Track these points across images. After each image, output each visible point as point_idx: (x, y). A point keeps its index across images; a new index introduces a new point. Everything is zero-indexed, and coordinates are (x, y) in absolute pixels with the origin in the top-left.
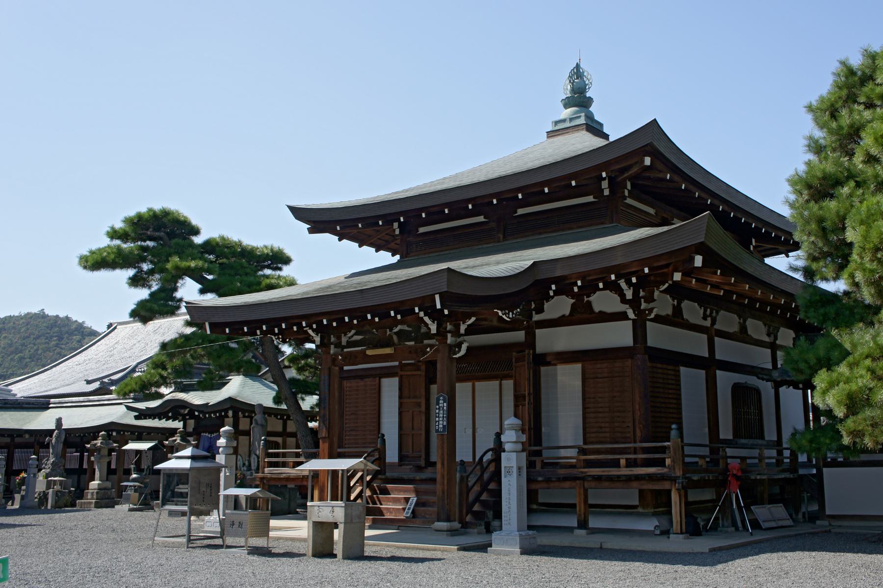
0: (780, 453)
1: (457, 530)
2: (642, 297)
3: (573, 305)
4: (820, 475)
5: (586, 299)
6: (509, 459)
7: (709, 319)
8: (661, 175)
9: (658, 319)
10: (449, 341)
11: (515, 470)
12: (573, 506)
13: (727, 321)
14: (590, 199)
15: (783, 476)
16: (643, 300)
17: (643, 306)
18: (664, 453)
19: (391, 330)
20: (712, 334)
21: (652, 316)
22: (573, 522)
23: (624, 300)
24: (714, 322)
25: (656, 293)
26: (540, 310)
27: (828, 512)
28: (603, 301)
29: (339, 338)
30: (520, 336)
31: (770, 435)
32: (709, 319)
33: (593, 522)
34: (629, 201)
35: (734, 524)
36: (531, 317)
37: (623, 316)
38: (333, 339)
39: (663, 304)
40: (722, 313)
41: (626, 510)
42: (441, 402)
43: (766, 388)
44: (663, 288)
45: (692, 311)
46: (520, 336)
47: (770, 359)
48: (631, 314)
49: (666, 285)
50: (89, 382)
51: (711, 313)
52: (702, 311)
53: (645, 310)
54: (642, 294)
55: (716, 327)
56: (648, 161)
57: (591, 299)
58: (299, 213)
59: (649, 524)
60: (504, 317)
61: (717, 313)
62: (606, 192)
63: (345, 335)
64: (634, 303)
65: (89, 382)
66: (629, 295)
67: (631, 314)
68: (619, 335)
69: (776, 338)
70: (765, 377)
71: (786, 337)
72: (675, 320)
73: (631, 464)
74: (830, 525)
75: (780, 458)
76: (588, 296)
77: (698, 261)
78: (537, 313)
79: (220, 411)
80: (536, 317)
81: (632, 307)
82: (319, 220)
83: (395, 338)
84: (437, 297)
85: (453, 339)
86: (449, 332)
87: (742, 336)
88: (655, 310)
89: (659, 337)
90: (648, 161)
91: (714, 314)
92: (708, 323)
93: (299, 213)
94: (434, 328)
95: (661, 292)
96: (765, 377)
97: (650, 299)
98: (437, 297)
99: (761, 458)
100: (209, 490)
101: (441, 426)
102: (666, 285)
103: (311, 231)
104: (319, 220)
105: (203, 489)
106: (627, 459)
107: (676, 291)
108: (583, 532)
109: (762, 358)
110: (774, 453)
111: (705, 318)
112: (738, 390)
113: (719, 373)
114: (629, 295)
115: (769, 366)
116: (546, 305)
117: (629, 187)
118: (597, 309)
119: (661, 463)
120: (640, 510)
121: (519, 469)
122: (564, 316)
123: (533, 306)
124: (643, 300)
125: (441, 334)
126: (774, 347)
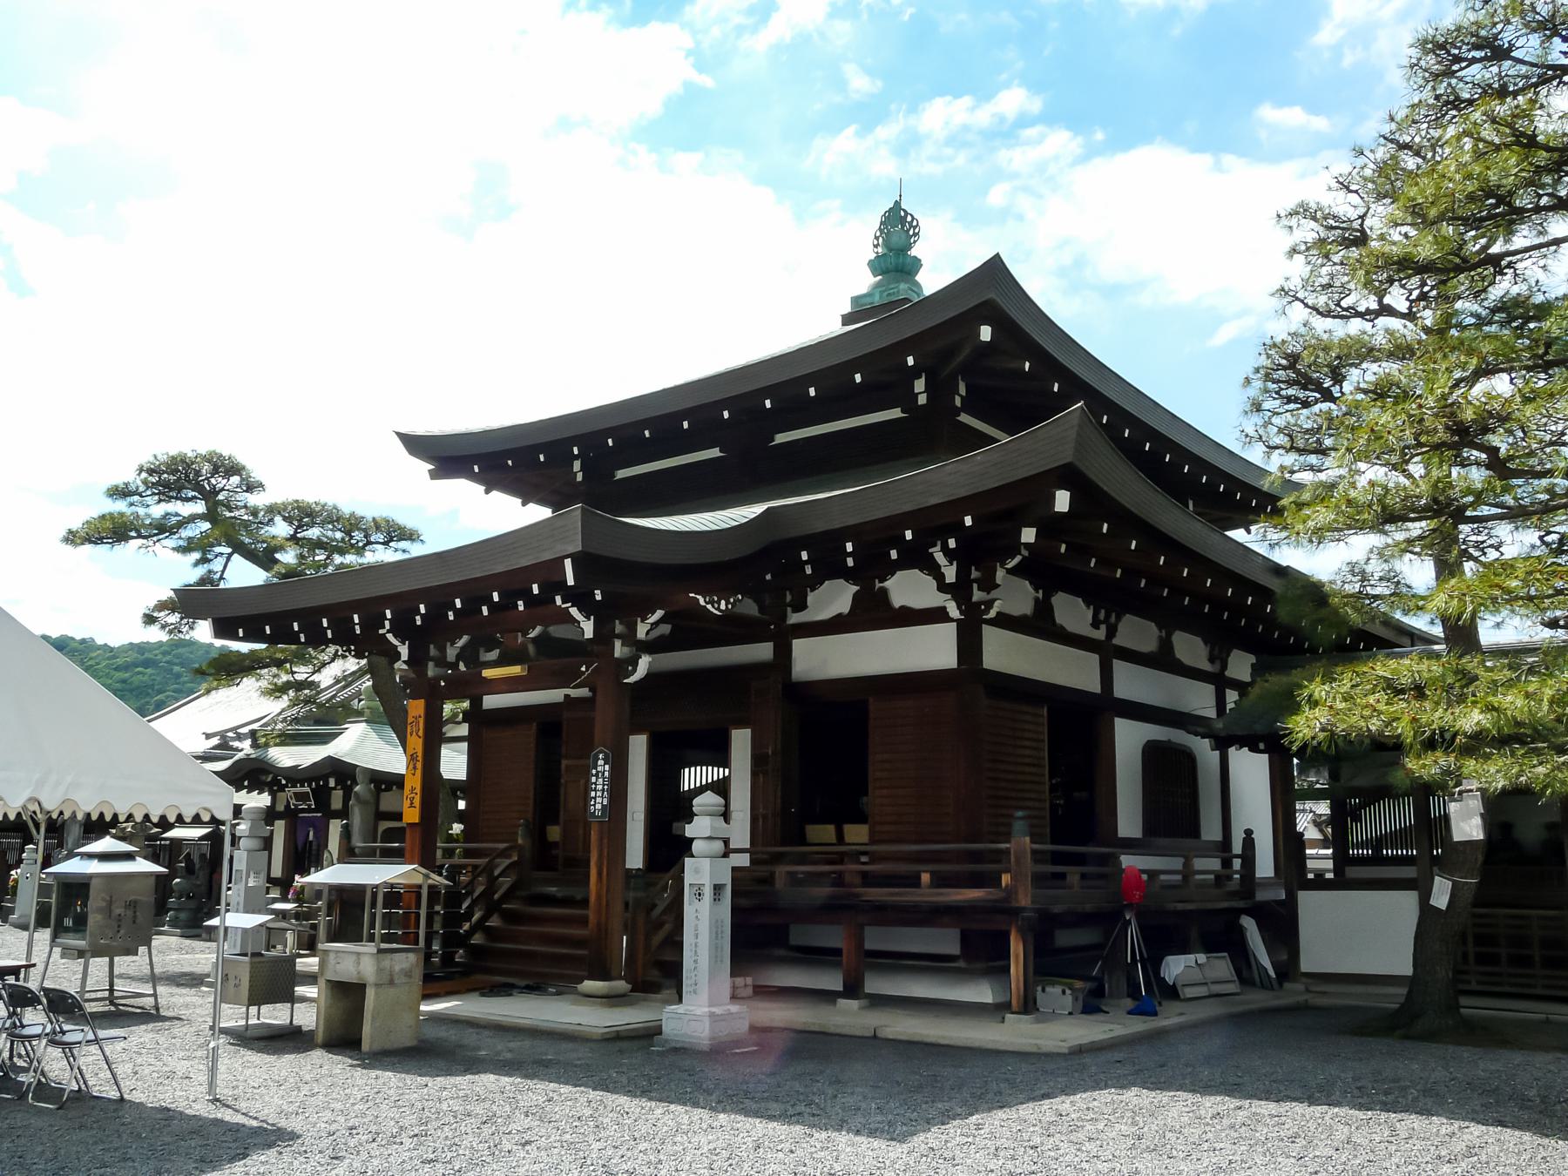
0: (1227, 863)
1: (624, 995)
2: (975, 581)
3: (856, 596)
4: (1291, 905)
5: (878, 585)
6: (697, 871)
7: (1103, 627)
8: (1013, 365)
9: (1003, 621)
10: (617, 654)
11: (708, 892)
12: (837, 952)
13: (1137, 633)
14: (895, 413)
15: (1225, 905)
16: (975, 586)
17: (977, 595)
18: (999, 862)
19: (525, 634)
20: (1108, 653)
21: (992, 614)
22: (832, 981)
23: (943, 587)
24: (1112, 632)
25: (1000, 574)
26: (801, 606)
27: (1306, 965)
28: (909, 588)
29: (443, 650)
30: (763, 651)
31: (1211, 830)
32: (1103, 627)
33: (876, 984)
34: (964, 418)
35: (1134, 992)
36: (784, 617)
37: (938, 615)
38: (433, 651)
39: (1015, 596)
40: (1128, 617)
41: (933, 964)
42: (601, 762)
43: (1203, 748)
44: (1011, 564)
45: (1072, 612)
46: (763, 651)
47: (1213, 702)
48: (954, 611)
49: (1018, 559)
50: (208, 736)
51: (1108, 616)
52: (1090, 613)
53: (979, 604)
54: (975, 574)
55: (1115, 641)
56: (986, 333)
57: (887, 584)
58: (416, 444)
59: (981, 993)
60: (709, 607)
61: (1119, 618)
62: (922, 400)
63: (453, 644)
64: (958, 591)
65: (208, 736)
66: (950, 574)
67: (954, 611)
68: (933, 649)
69: (1224, 667)
70: (1200, 730)
71: (1240, 666)
72: (1040, 624)
73: (940, 881)
74: (1308, 991)
75: (1228, 872)
76: (883, 580)
77: (1062, 501)
78: (795, 611)
79: (317, 779)
80: (794, 618)
81: (954, 598)
82: (450, 456)
83: (531, 649)
84: (568, 563)
85: (626, 649)
86: (618, 637)
87: (1162, 660)
88: (997, 603)
89: (1005, 653)
90: (986, 333)
91: (1113, 619)
92: (1100, 634)
93: (416, 444)
94: (588, 628)
95: (1009, 571)
96: (1200, 730)
97: (989, 584)
98: (568, 563)
99: (1187, 872)
100: (130, 913)
101: (599, 806)
102: (1018, 559)
103: (434, 475)
104: (450, 456)
105: (118, 911)
106: (932, 873)
107: (1037, 569)
108: (853, 1004)
109: (1199, 699)
110: (1214, 864)
111: (1095, 624)
112: (1154, 754)
113: (1119, 722)
114: (950, 574)
115: (1211, 713)
116: (811, 598)
117: (962, 390)
118: (897, 601)
119: (992, 881)
120: (961, 964)
121: (718, 889)
122: (840, 615)
123: (789, 598)
124: (975, 586)
125: (604, 636)
126: (1221, 682)
